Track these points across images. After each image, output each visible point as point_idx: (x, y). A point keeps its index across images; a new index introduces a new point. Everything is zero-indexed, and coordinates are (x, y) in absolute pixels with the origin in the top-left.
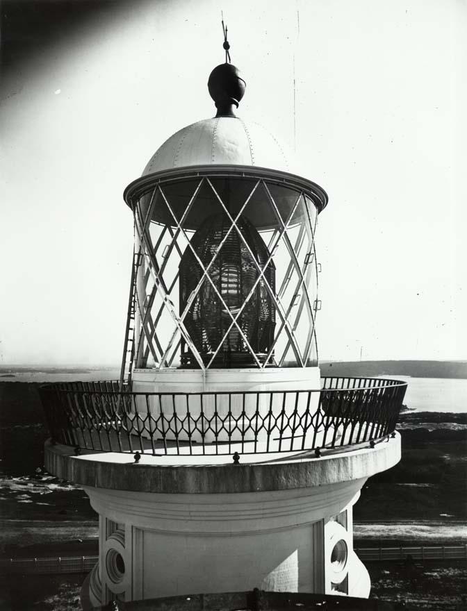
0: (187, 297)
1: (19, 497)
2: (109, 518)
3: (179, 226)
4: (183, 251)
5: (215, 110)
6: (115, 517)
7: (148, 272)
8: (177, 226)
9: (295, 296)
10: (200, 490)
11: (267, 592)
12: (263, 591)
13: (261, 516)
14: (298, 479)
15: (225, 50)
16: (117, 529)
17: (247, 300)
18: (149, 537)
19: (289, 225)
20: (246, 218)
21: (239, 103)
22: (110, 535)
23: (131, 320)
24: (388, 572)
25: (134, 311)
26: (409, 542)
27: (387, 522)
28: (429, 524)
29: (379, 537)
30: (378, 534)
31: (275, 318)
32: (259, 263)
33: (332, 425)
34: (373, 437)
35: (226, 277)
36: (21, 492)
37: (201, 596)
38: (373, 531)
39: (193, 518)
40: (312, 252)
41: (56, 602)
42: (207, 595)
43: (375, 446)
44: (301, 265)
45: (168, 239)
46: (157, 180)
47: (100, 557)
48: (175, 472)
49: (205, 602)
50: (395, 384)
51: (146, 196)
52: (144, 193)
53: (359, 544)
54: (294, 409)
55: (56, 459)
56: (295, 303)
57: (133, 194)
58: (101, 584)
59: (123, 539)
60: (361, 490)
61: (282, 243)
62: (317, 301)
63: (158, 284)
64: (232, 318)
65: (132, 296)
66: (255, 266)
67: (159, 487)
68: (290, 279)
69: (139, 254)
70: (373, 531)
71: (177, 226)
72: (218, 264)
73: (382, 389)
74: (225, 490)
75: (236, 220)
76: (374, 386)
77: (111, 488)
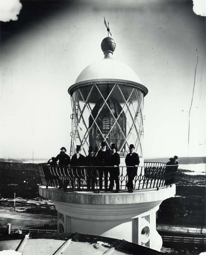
1: (50, 207)
5: (104, 56)
10: (86, 202)
14: (123, 200)
21: (113, 53)
22: (60, 218)
24: (197, 248)
29: (194, 233)
30: (194, 232)
33: (146, 180)
34: (158, 186)
36: (51, 205)
38: (192, 230)
43: (159, 190)
44: (134, 117)
46: (77, 86)
48: (76, 196)
52: (74, 91)
54: (140, 173)
57: (71, 91)
59: (64, 220)
70: (192, 230)
76: (161, 165)
77: (56, 201)
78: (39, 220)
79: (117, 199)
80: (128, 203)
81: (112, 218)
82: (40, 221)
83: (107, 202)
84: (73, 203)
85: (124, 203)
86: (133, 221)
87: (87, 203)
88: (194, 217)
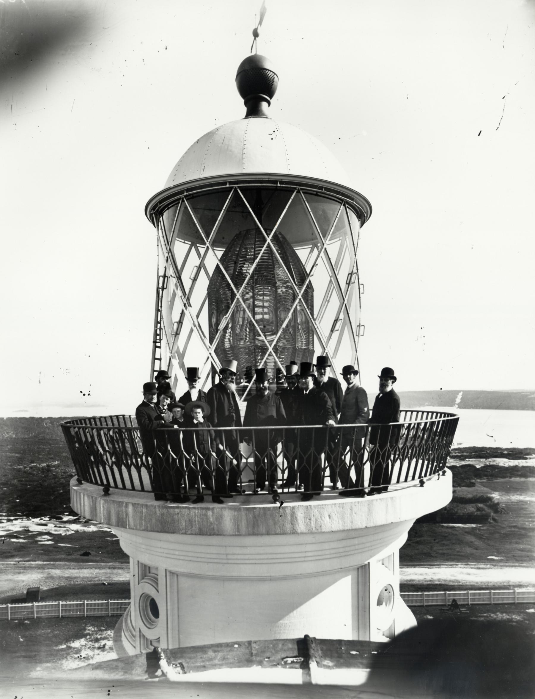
0: (218, 324)
1: (39, 538)
2: (141, 561)
3: (208, 244)
4: (211, 272)
5: (244, 110)
6: (146, 559)
7: (174, 295)
8: (205, 244)
9: (336, 321)
10: (239, 531)
11: (318, 640)
12: (314, 638)
13: (303, 559)
15: (253, 38)
16: (149, 573)
17: (284, 325)
18: (182, 580)
19: (329, 240)
20: (280, 233)
22: (143, 579)
23: (157, 349)
25: (160, 340)
26: (454, 586)
27: (431, 565)
28: (476, 566)
29: (422, 580)
31: (313, 345)
32: (296, 284)
34: (423, 475)
35: (260, 300)
36: (41, 534)
37: (250, 643)
39: (230, 561)
40: (355, 271)
41: (82, 646)
42: (255, 642)
43: (424, 485)
44: (343, 286)
45: (194, 260)
46: (182, 192)
47: (132, 601)
49: (253, 649)
50: (444, 417)
51: (170, 210)
52: (167, 207)
53: (405, 587)
55: (84, 498)
56: (336, 328)
58: (135, 630)
59: (157, 584)
60: (409, 533)
61: (322, 263)
62: (359, 326)
63: (186, 308)
64: (268, 345)
65: (157, 322)
66: (292, 288)
67: (194, 528)
68: (329, 302)
69: (165, 276)
71: (205, 244)
72: (252, 286)
73: (439, 422)
74: (264, 531)
75: (209, 240)
77: (144, 530)
78: (10, 577)
79: (327, 518)
80: (357, 527)
81: (309, 567)
82: (10, 580)
83: (301, 527)
84: (200, 535)
85: (346, 528)
86: (355, 573)
87: (244, 533)
88: (418, 539)
